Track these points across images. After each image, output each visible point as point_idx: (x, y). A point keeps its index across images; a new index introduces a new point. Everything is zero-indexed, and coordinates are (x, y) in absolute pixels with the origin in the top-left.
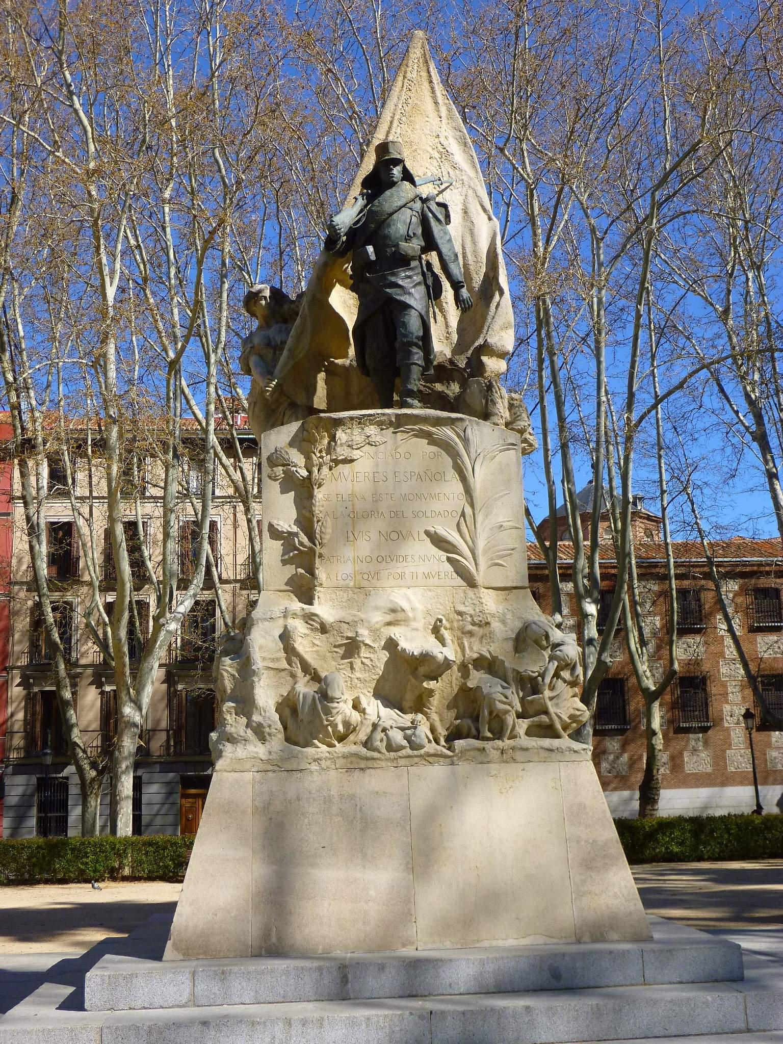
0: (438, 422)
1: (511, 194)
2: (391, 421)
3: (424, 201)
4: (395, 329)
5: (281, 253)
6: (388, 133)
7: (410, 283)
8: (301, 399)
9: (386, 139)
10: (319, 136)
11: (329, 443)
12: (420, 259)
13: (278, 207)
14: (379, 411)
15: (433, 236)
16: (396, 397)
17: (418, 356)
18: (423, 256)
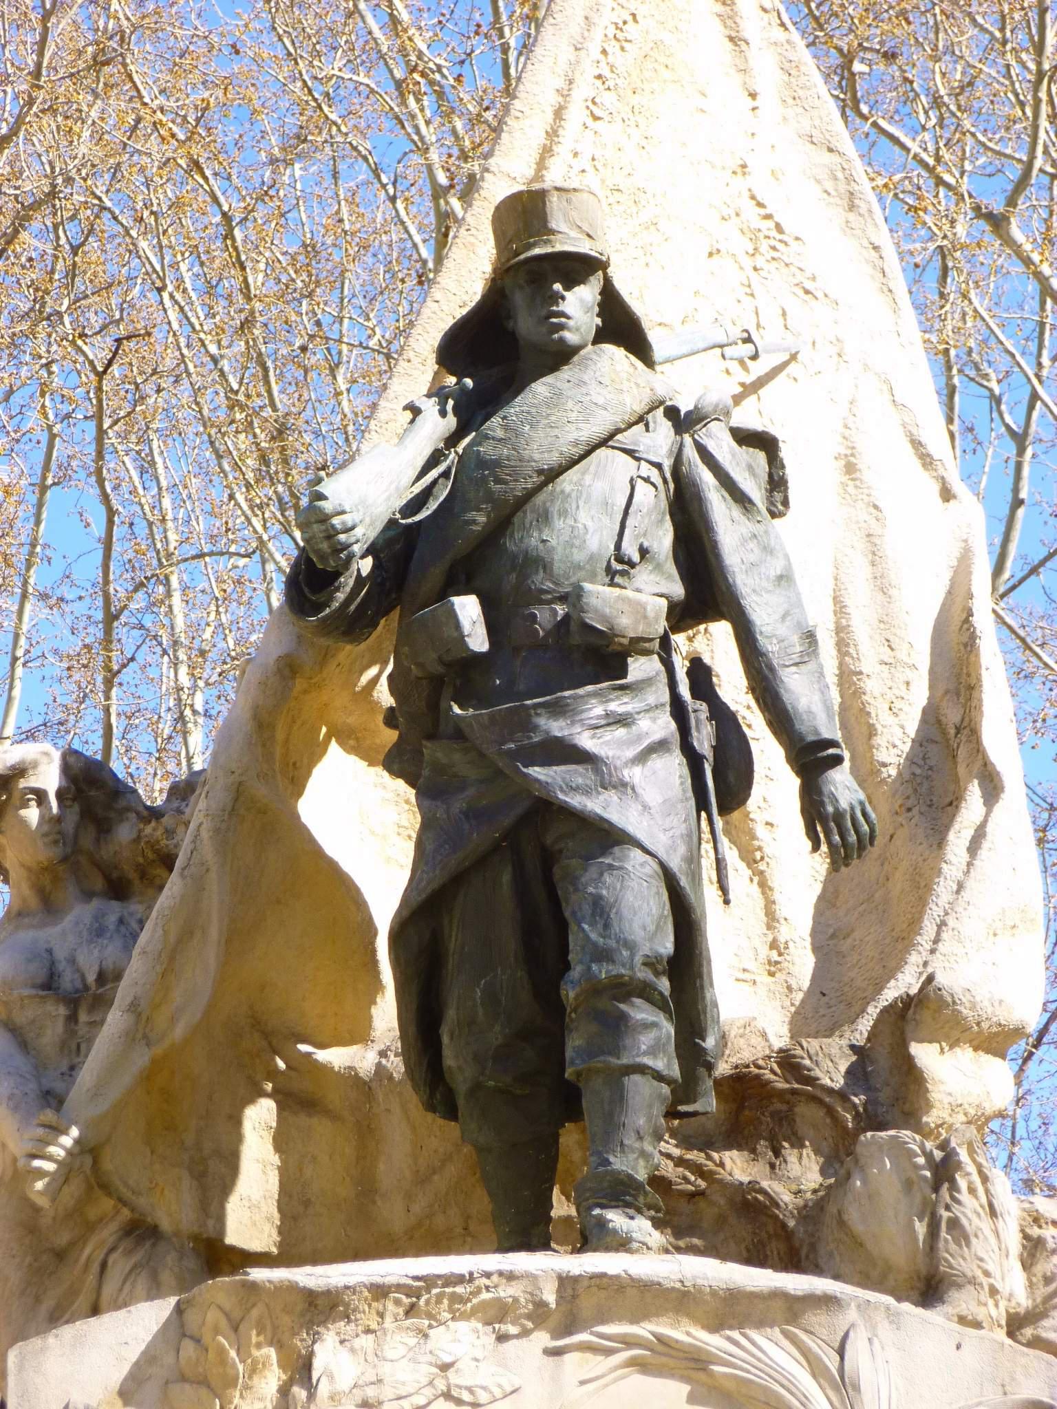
0: (731, 1310)
1: (1035, 397)
2: (541, 1305)
3: (683, 422)
4: (562, 927)
5: (111, 618)
6: (546, 152)
7: (622, 744)
8: (172, 1210)
9: (538, 177)
10: (273, 161)
11: (284, 1391)
12: (665, 642)
13: (101, 433)
14: (359, 600)
15: (718, 556)
16: (561, 1207)
17: (652, 1036)
18: (679, 639)
